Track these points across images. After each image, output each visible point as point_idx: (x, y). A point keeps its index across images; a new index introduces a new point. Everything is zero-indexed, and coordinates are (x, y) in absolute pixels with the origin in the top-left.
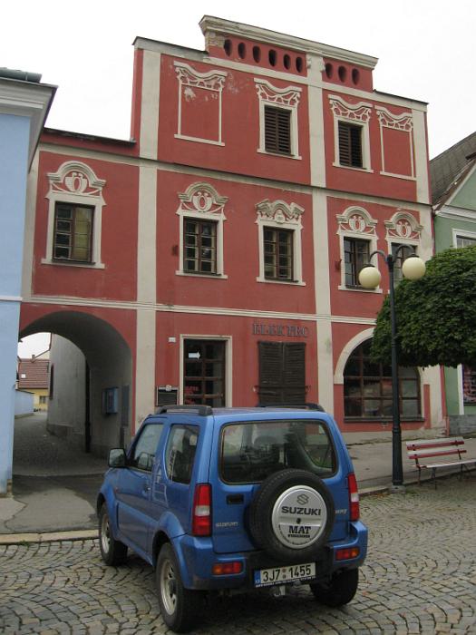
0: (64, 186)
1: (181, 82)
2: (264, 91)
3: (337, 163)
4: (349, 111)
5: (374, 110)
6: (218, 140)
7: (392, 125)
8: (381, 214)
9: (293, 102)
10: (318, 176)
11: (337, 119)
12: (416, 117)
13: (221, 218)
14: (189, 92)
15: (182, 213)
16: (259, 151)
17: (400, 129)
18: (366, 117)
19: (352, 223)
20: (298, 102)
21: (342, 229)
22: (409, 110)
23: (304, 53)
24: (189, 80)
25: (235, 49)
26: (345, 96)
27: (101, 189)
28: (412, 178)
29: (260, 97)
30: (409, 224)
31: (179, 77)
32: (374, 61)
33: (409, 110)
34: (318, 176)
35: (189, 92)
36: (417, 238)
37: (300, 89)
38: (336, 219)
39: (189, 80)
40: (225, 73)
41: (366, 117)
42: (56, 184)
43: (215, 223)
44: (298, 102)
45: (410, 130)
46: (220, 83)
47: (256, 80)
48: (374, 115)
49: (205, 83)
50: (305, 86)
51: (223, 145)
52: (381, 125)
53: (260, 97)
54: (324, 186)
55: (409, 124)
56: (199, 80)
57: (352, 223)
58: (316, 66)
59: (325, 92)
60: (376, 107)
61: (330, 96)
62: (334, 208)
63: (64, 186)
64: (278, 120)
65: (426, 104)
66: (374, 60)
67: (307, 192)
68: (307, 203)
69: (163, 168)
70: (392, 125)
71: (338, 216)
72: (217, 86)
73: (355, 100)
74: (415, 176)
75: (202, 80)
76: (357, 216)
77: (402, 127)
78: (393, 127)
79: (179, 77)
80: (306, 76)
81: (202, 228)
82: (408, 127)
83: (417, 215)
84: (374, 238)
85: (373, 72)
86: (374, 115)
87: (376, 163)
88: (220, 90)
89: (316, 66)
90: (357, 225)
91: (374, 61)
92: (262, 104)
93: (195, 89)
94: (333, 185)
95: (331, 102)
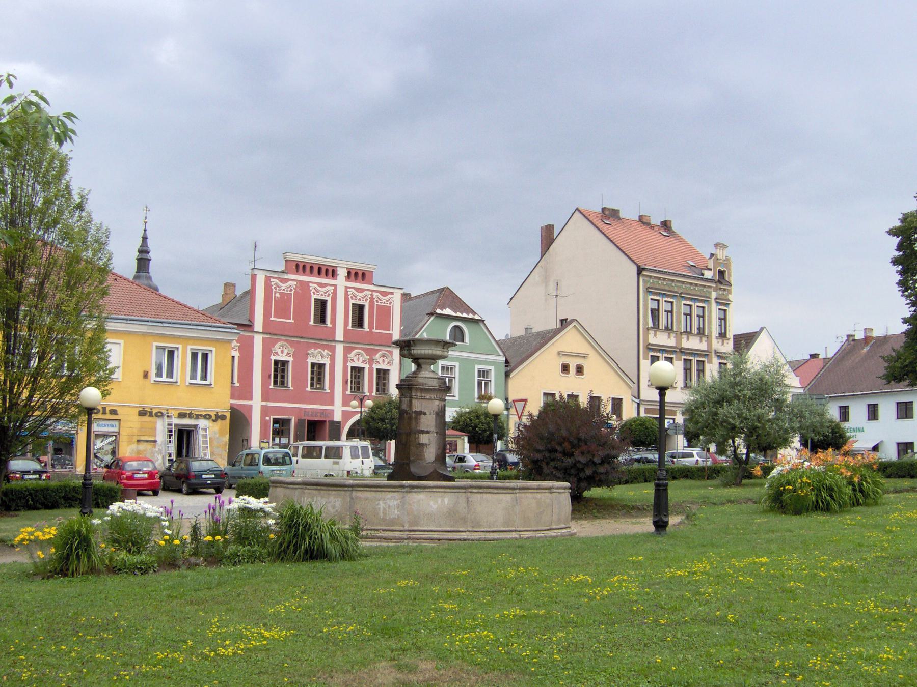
0: (353, 360)
1: (274, 290)
2: (314, 291)
3: (350, 327)
5: (372, 295)
8: (371, 353)
10: (339, 336)
11: (351, 302)
13: (291, 359)
14: (278, 295)
15: (273, 358)
16: (310, 323)
22: (392, 293)
26: (357, 289)
28: (391, 332)
34: (339, 336)
35: (278, 295)
37: (333, 288)
40: (295, 283)
47: (311, 285)
48: (372, 298)
50: (335, 286)
51: (293, 321)
52: (376, 303)
58: (342, 273)
59: (346, 287)
60: (374, 293)
61: (349, 290)
64: (321, 305)
67: (333, 344)
68: (333, 350)
71: (349, 356)
72: (291, 290)
78: (382, 304)
80: (336, 279)
82: (391, 303)
86: (372, 298)
87: (371, 327)
88: (293, 292)
89: (342, 273)
92: (313, 297)
93: (280, 293)
94: (268, 329)
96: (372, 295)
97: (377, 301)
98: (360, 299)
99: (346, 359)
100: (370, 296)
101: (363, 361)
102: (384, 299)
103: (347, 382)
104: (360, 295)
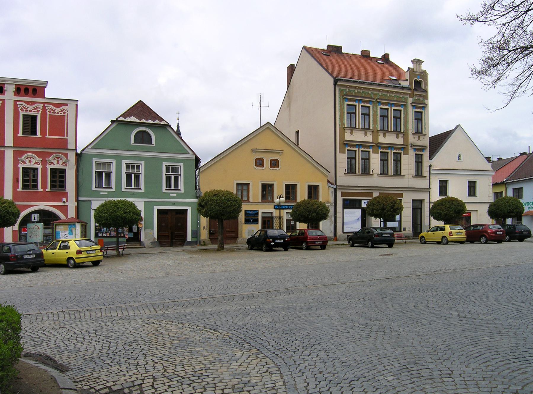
0: (53, 163)
3: (20, 134)
4: (29, 109)
5: (44, 107)
6: (65, 136)
7: (55, 113)
8: (44, 156)
9: (38, 111)
12: (71, 109)
17: (60, 114)
18: (39, 111)
19: (27, 161)
20: (41, 111)
21: (21, 164)
22: (67, 105)
23: (4, 84)
24: (52, 112)
25: (22, 91)
26: (27, 102)
27: (40, 162)
28: (66, 137)
29: (20, 111)
30: (61, 159)
31: (47, 111)
32: (46, 83)
33: (67, 105)
36: (66, 165)
38: (19, 160)
39: (52, 112)
41: (39, 111)
42: (22, 162)
43: (37, 169)
44: (41, 111)
45: (66, 114)
46: (40, 109)
48: (44, 110)
49: (59, 112)
52: (48, 113)
53: (20, 111)
54: (12, 146)
55: (66, 111)
56: (57, 111)
57: (55, 162)
58: (10, 90)
59: (15, 101)
60: (46, 105)
61: (18, 103)
62: (17, 155)
63: (53, 163)
65: (78, 100)
66: (46, 83)
67: (2, 149)
69: (15, 149)
70: (55, 113)
73: (33, 103)
74: (67, 136)
75: (58, 111)
76: (30, 158)
77: (61, 113)
79: (47, 111)
80: (4, 95)
81: (32, 171)
82: (65, 113)
83: (66, 155)
84: (40, 167)
85: (46, 89)
86: (44, 110)
87: (43, 132)
89: (10, 90)
90: (58, 162)
91: (46, 83)
95: (19, 106)
96: (44, 107)
97: (50, 112)
98: (31, 111)
99: (16, 162)
100: (42, 108)
101: (36, 163)
102: (57, 110)
103: (18, 181)
104: (30, 107)
